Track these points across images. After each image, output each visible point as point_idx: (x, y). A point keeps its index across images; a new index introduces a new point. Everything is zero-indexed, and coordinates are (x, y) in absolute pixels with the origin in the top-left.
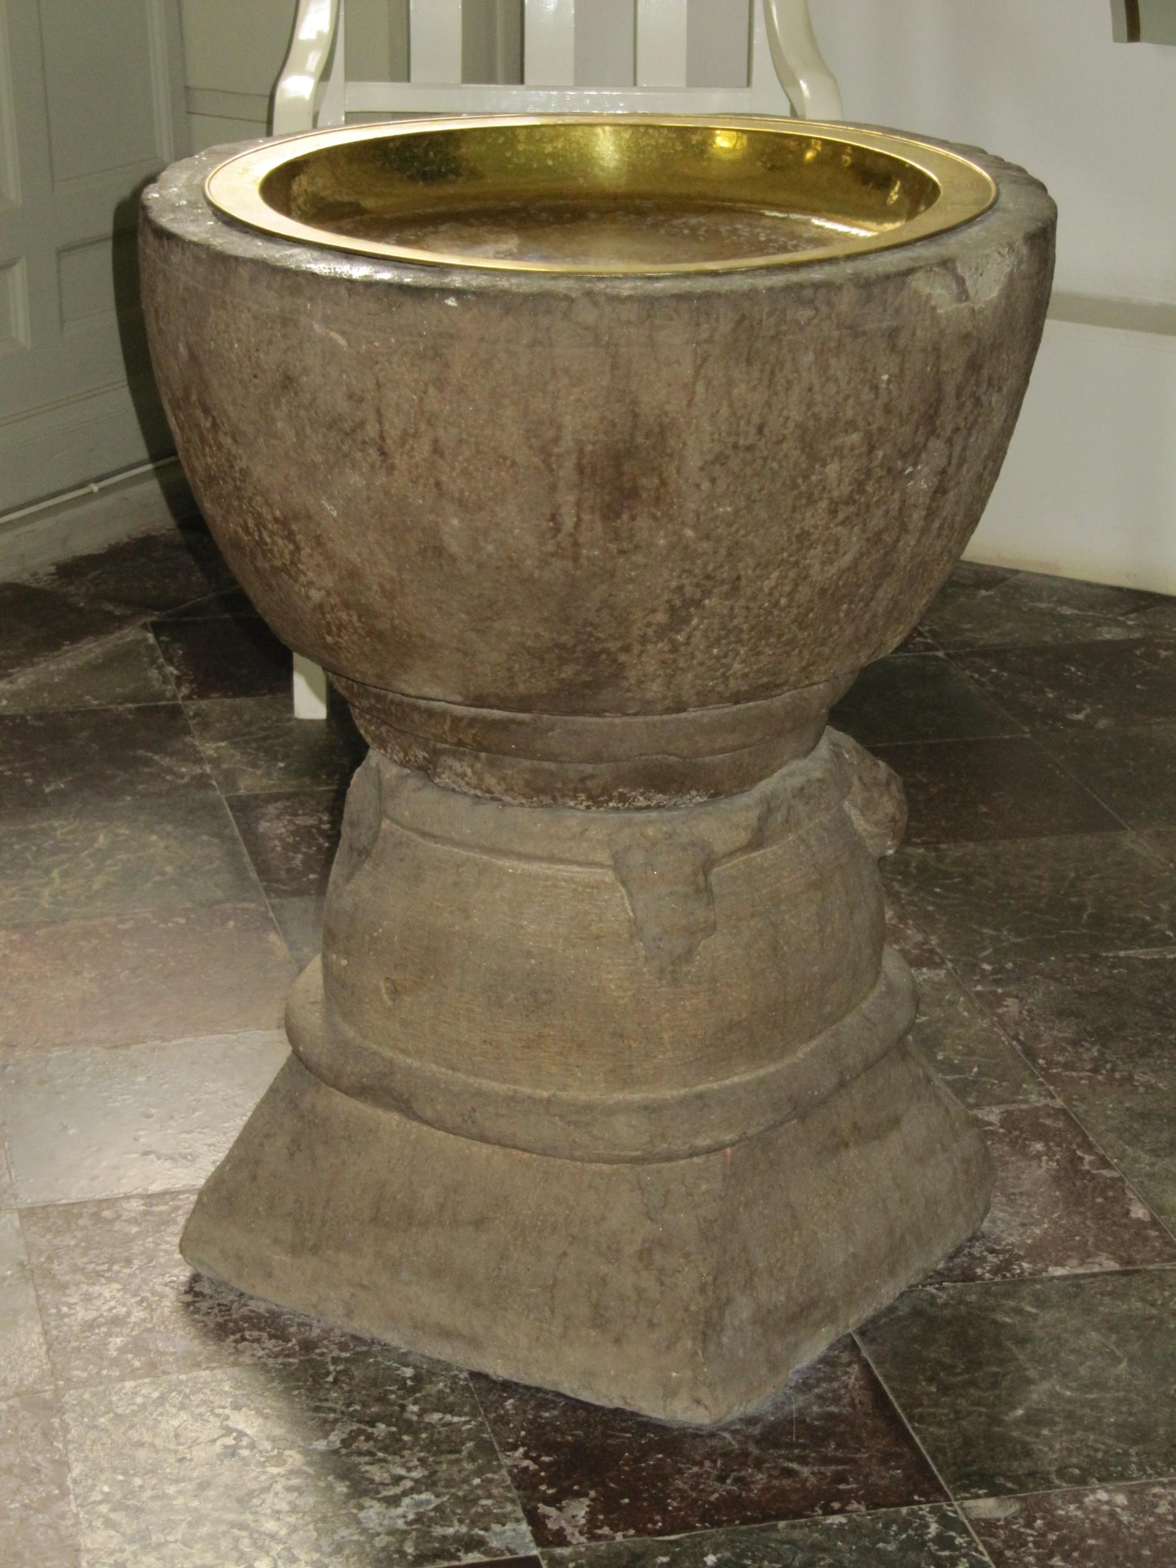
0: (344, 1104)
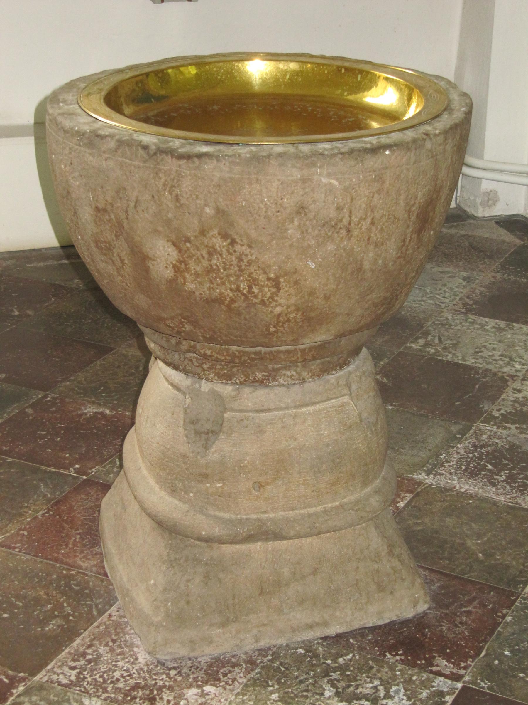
0: (228, 549)
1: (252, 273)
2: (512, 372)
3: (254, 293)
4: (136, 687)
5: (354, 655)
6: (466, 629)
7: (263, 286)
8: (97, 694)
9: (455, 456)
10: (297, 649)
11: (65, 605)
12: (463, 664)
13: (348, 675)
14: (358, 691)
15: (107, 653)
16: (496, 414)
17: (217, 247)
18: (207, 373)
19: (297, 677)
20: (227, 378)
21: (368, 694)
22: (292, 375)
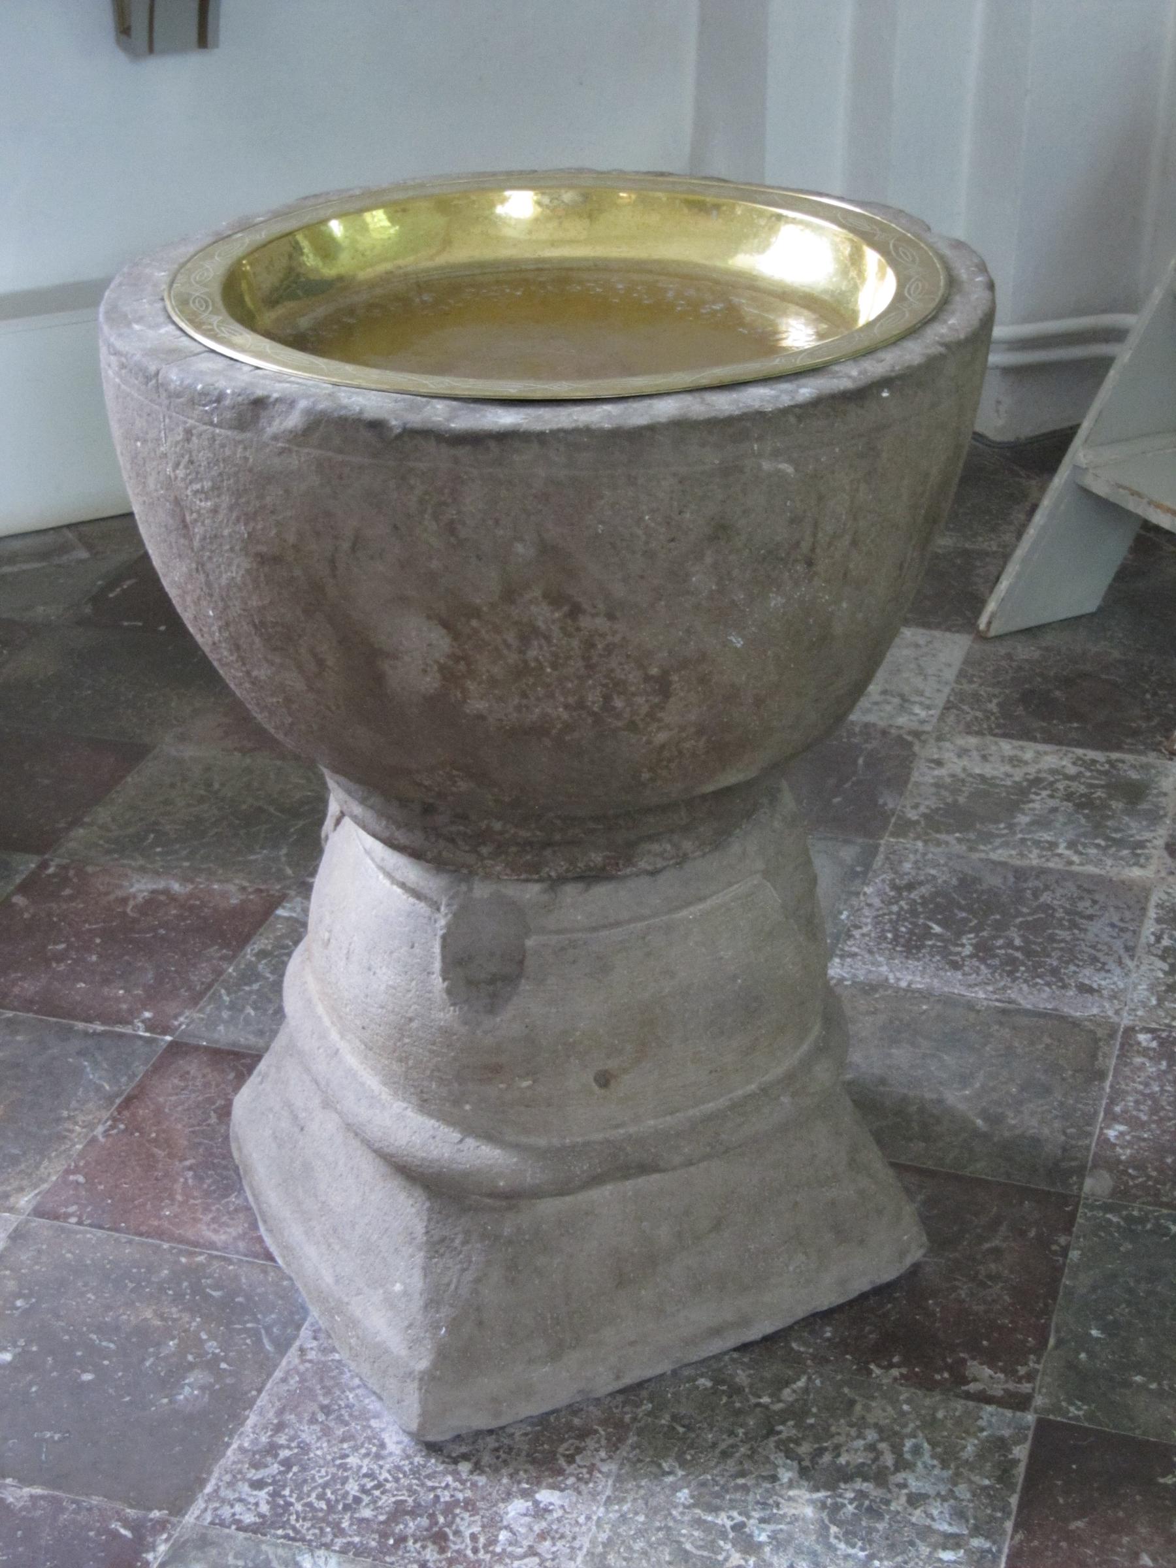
0: (548, 1207)
1: (612, 670)
2: (915, 726)
3: (614, 708)
4: (399, 1512)
5: (809, 1379)
6: (1002, 1288)
7: (634, 695)
8: (324, 1540)
9: (866, 911)
10: (695, 1380)
11: (204, 1336)
12: (1022, 1371)
13: (812, 1425)
14: (842, 1460)
15: (319, 1439)
16: (913, 815)
17: (540, 623)
18: (489, 862)
19: (714, 1445)
20: (531, 871)
21: (863, 1464)
22: (665, 851)
